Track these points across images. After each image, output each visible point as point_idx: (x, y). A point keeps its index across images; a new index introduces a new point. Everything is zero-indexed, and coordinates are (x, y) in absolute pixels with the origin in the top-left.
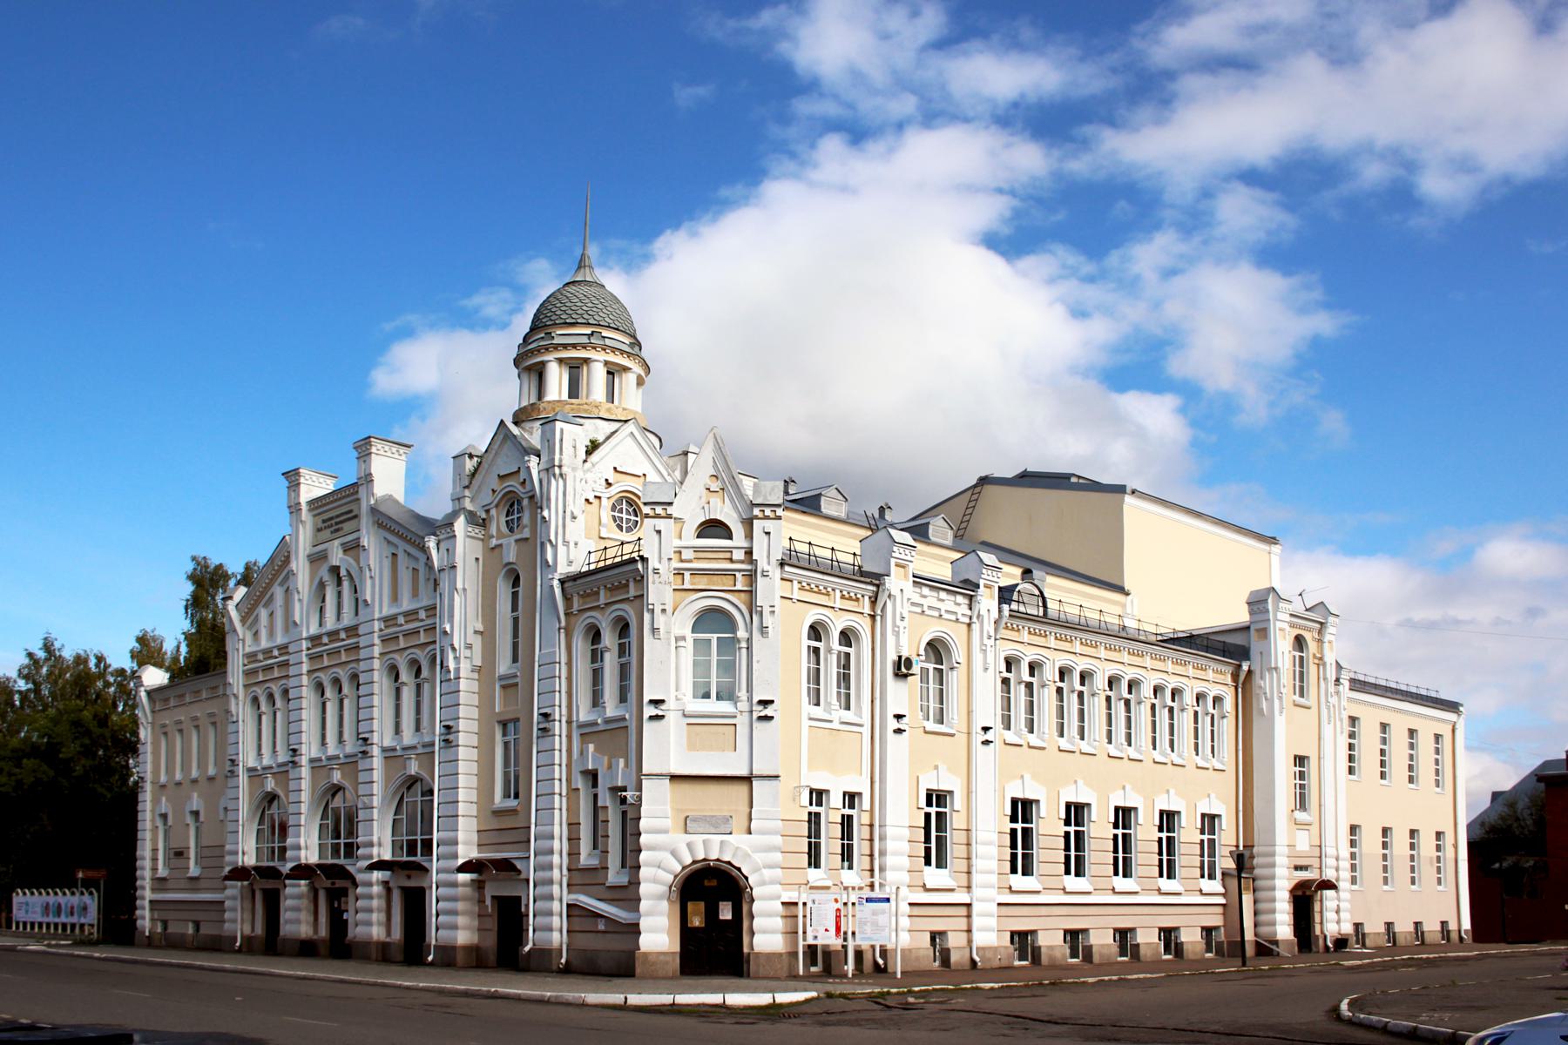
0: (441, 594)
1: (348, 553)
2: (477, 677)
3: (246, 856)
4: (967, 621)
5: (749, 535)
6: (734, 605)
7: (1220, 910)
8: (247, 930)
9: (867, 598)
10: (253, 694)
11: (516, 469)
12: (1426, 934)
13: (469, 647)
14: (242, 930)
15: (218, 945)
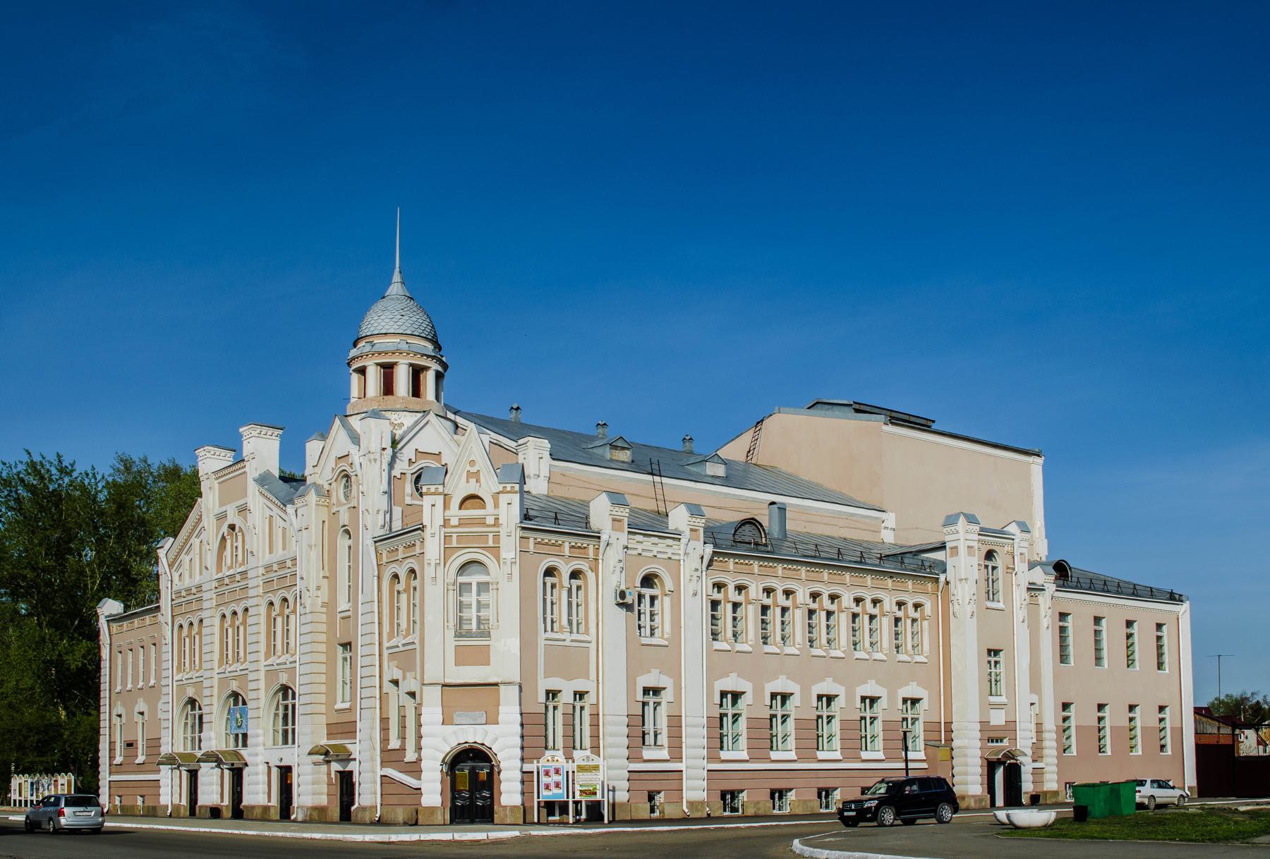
5: (496, 506)
10: (221, 612)
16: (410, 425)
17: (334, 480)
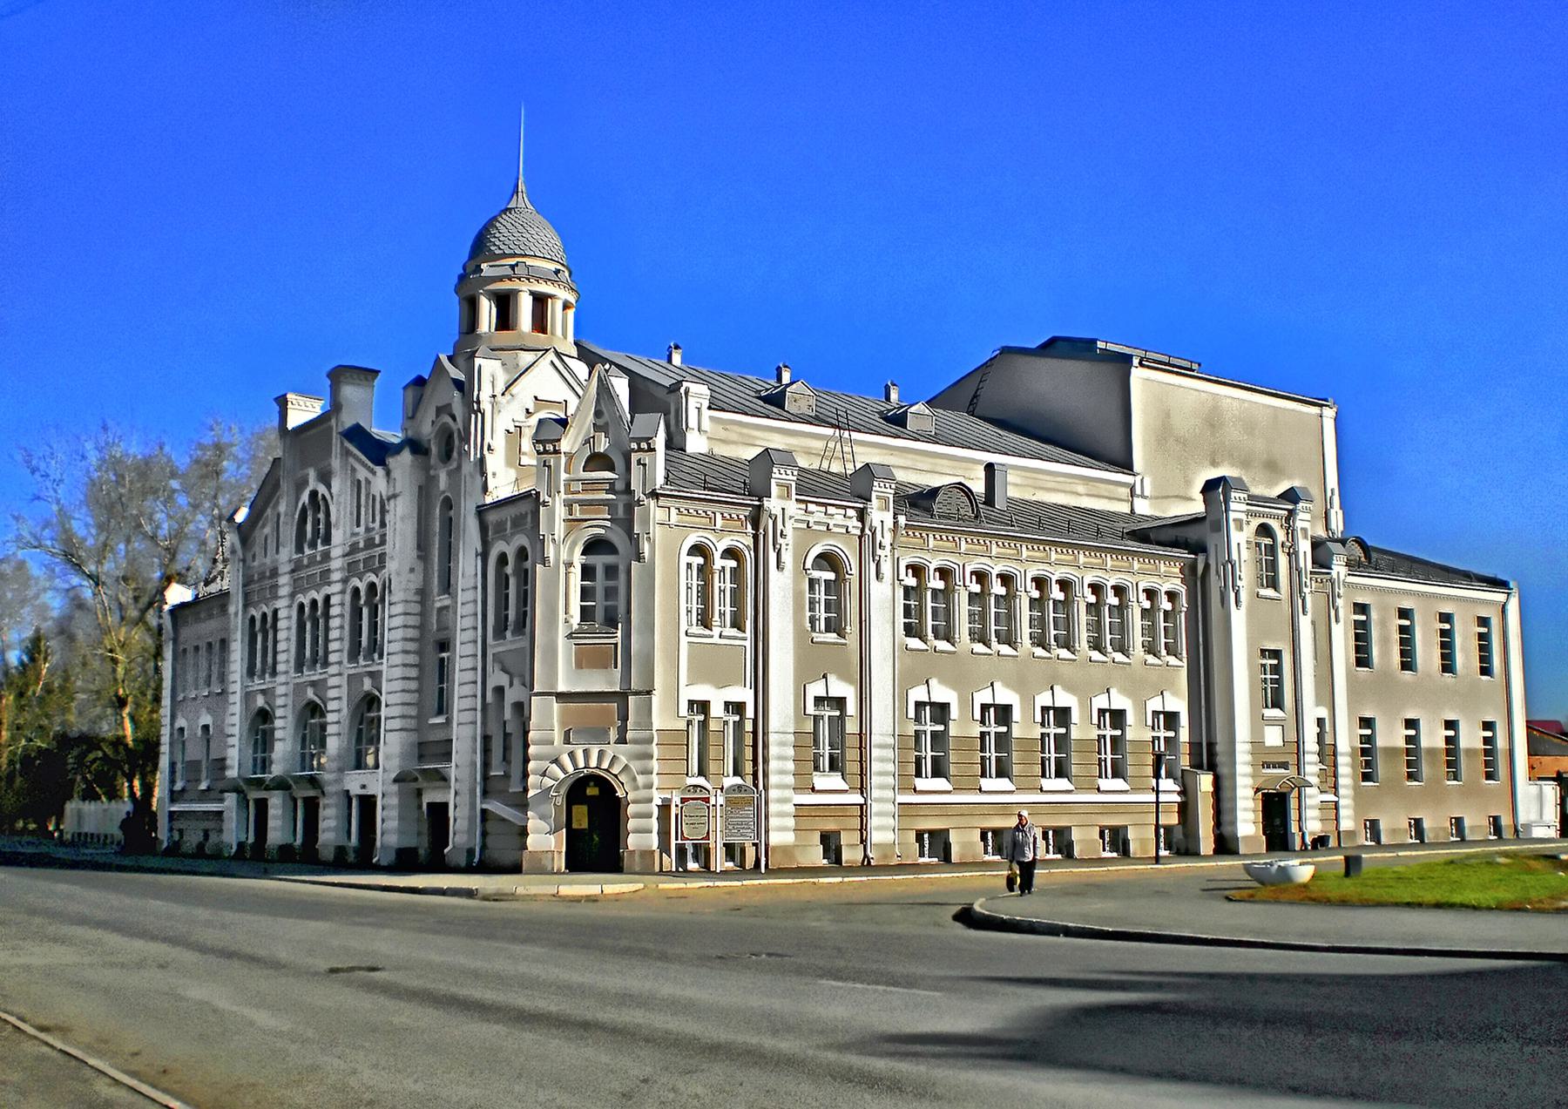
6: (618, 538)
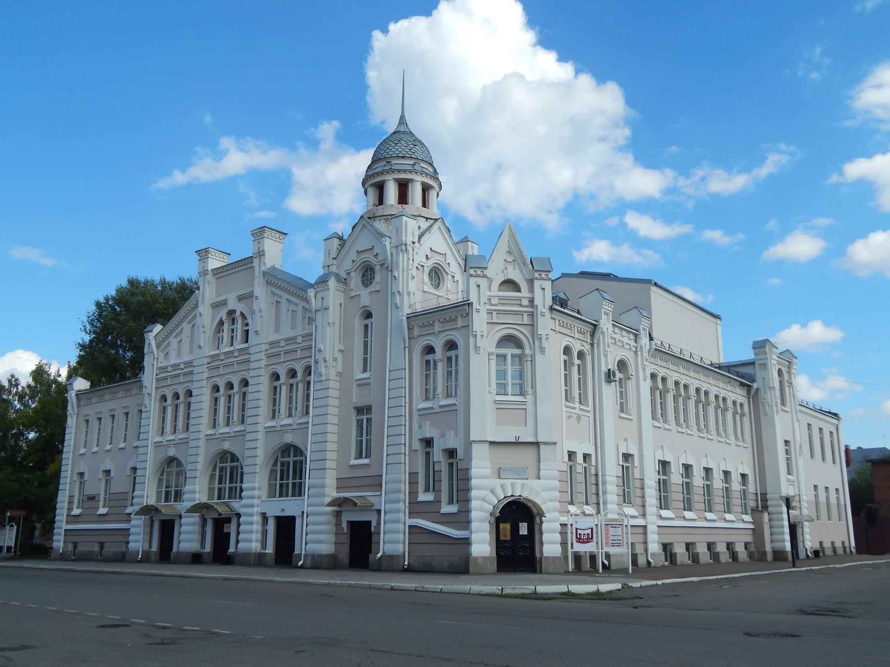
0: (316, 326)
1: (241, 301)
2: (339, 380)
3: (149, 499)
4: (635, 350)
6: (523, 334)
7: (750, 532)
8: (146, 547)
9: (589, 332)
11: (371, 247)
12: (837, 549)
13: (335, 359)
14: (142, 547)
15: (123, 558)
16: (425, 228)
17: (353, 270)
